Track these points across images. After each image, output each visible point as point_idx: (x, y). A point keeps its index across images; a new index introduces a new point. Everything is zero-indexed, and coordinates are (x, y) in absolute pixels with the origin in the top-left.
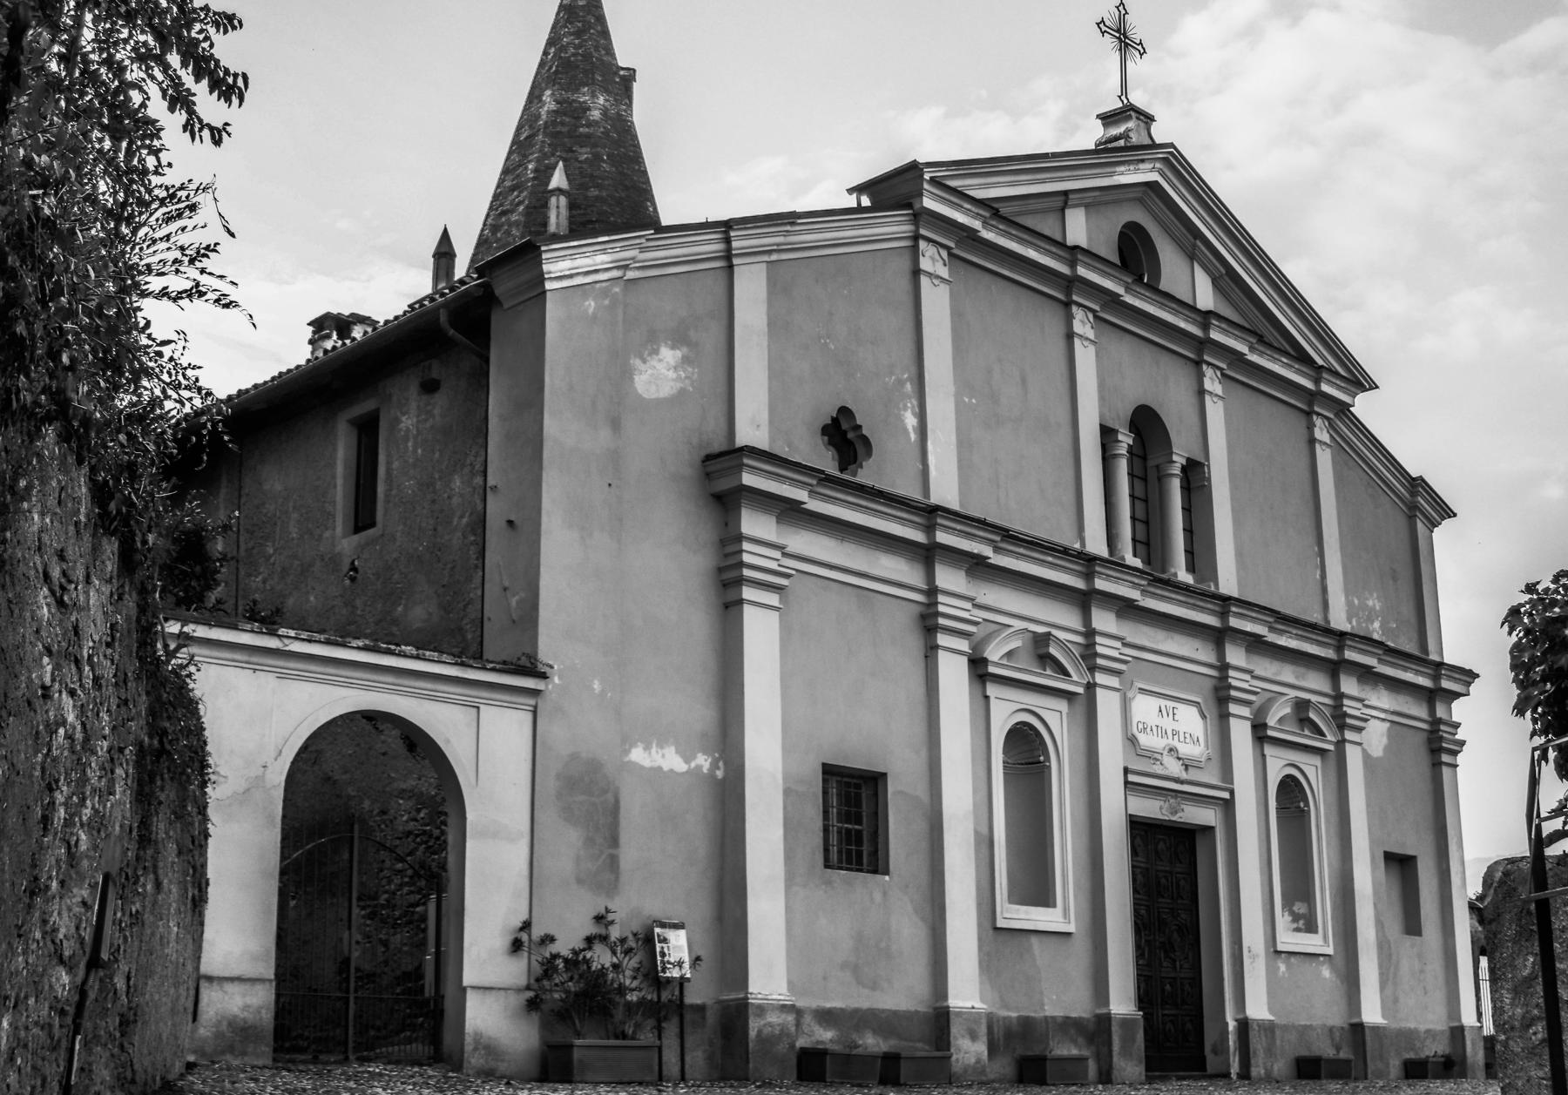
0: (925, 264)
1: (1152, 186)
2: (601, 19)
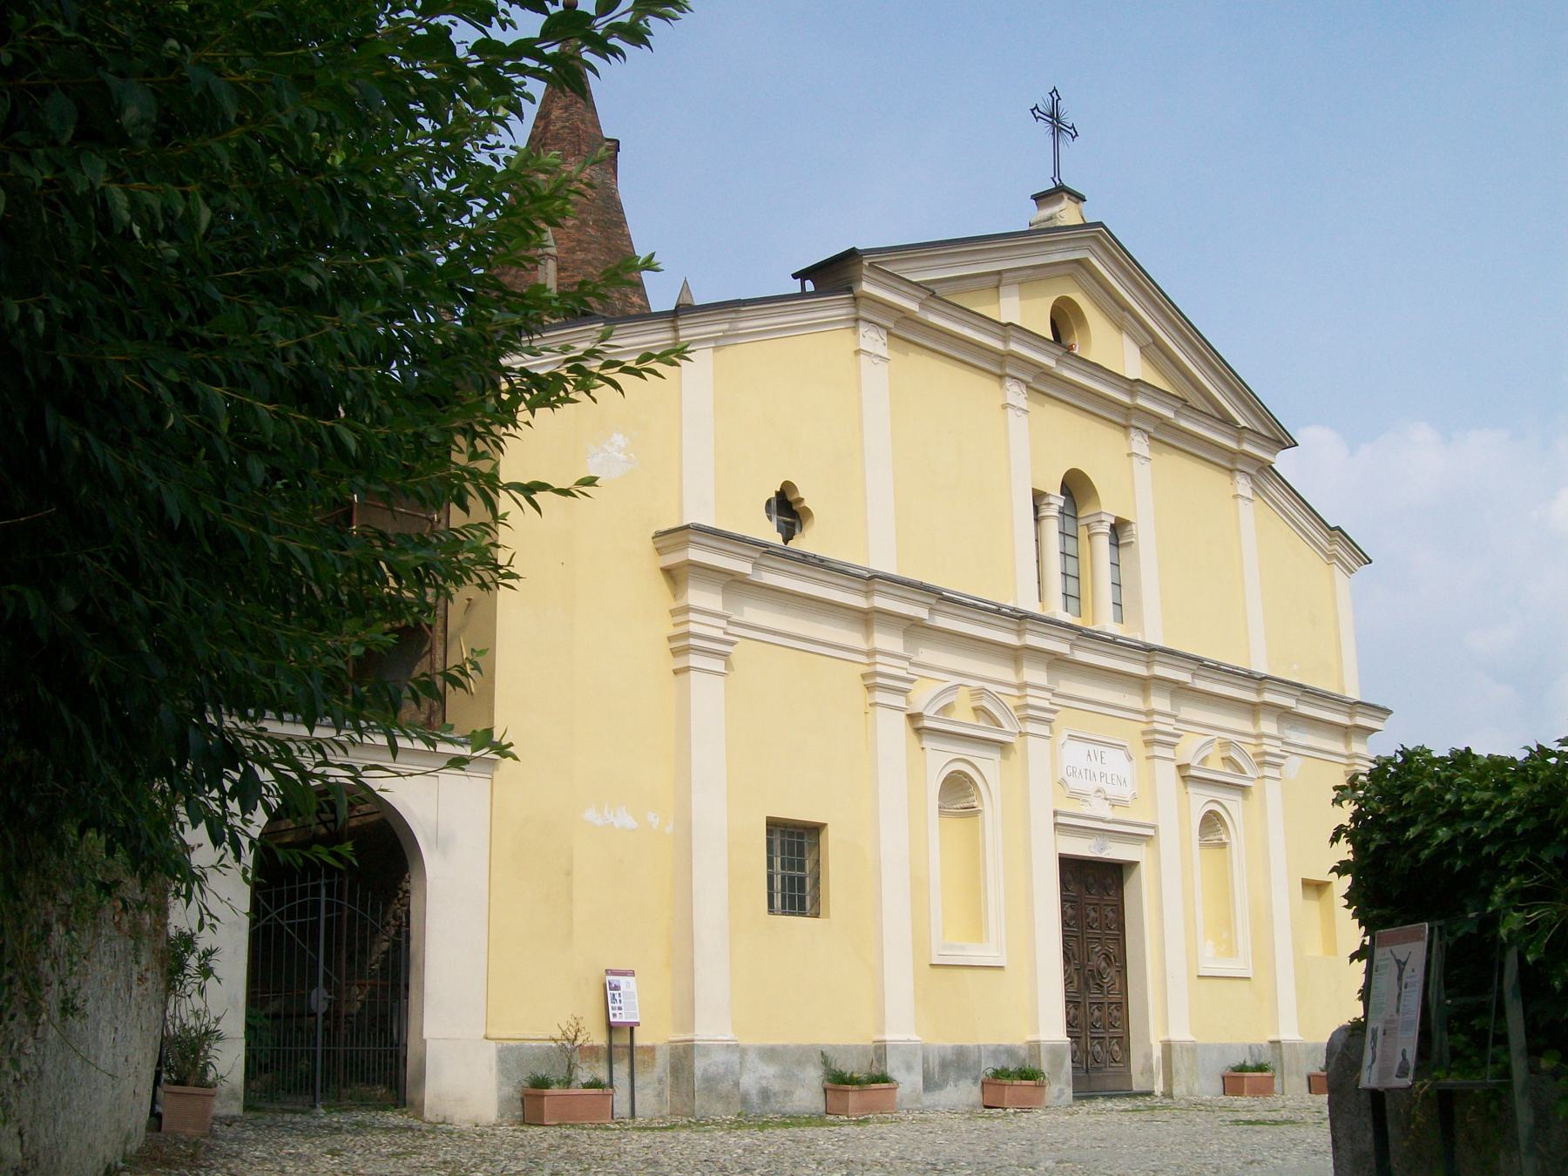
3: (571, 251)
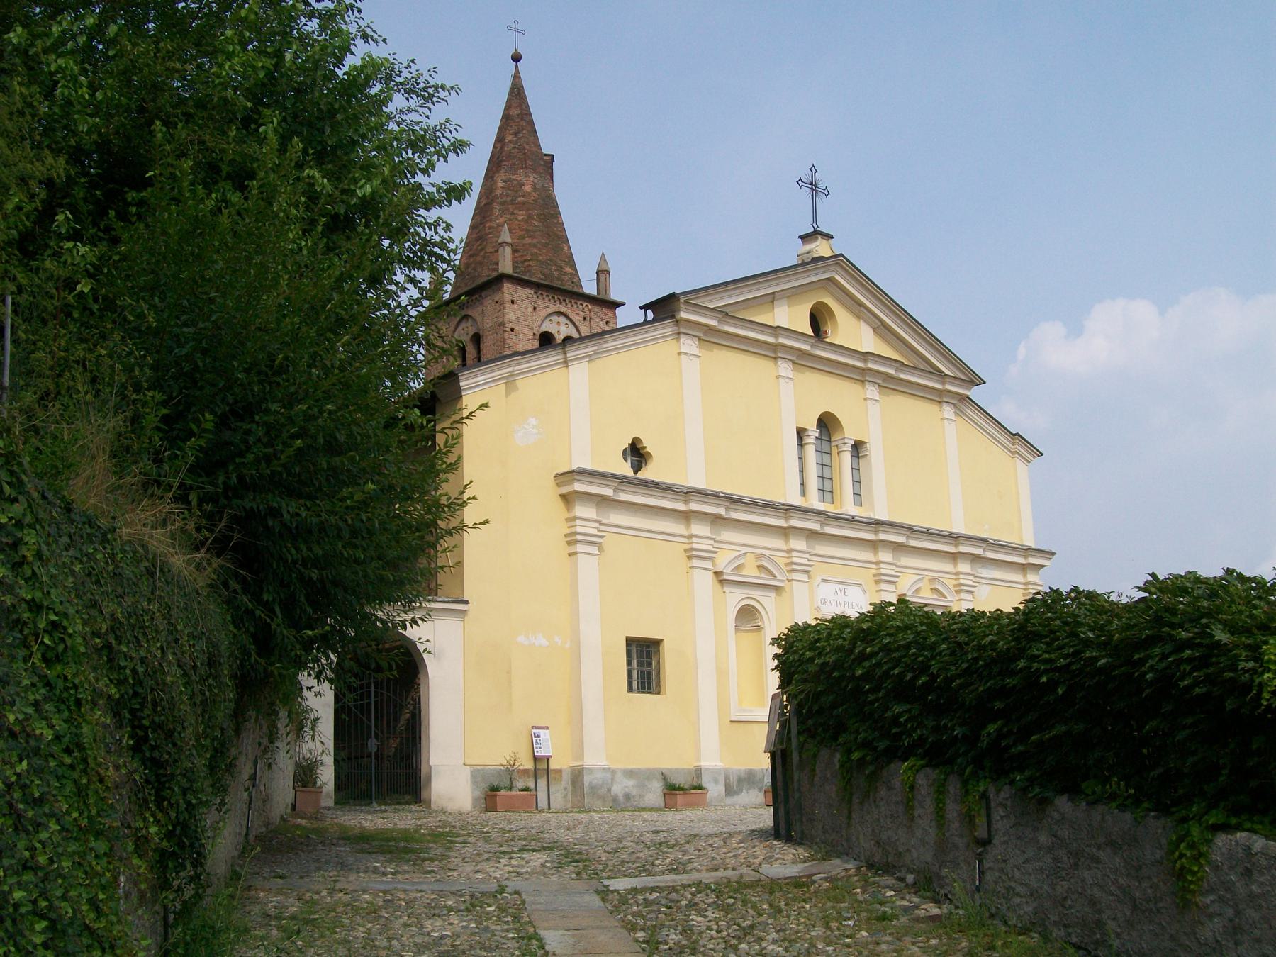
2: (531, 123)
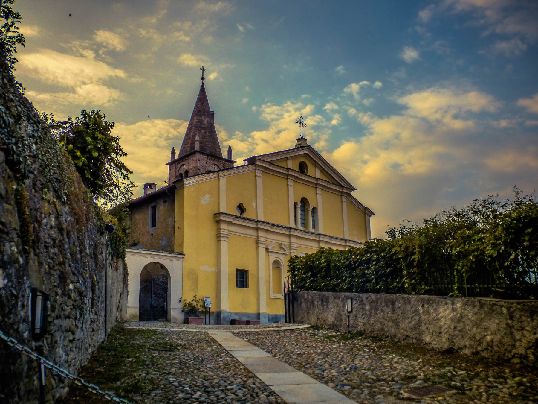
0: (257, 174)
1: (306, 154)
2: (207, 101)
3: (203, 139)
